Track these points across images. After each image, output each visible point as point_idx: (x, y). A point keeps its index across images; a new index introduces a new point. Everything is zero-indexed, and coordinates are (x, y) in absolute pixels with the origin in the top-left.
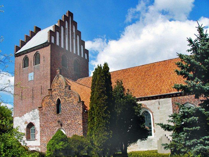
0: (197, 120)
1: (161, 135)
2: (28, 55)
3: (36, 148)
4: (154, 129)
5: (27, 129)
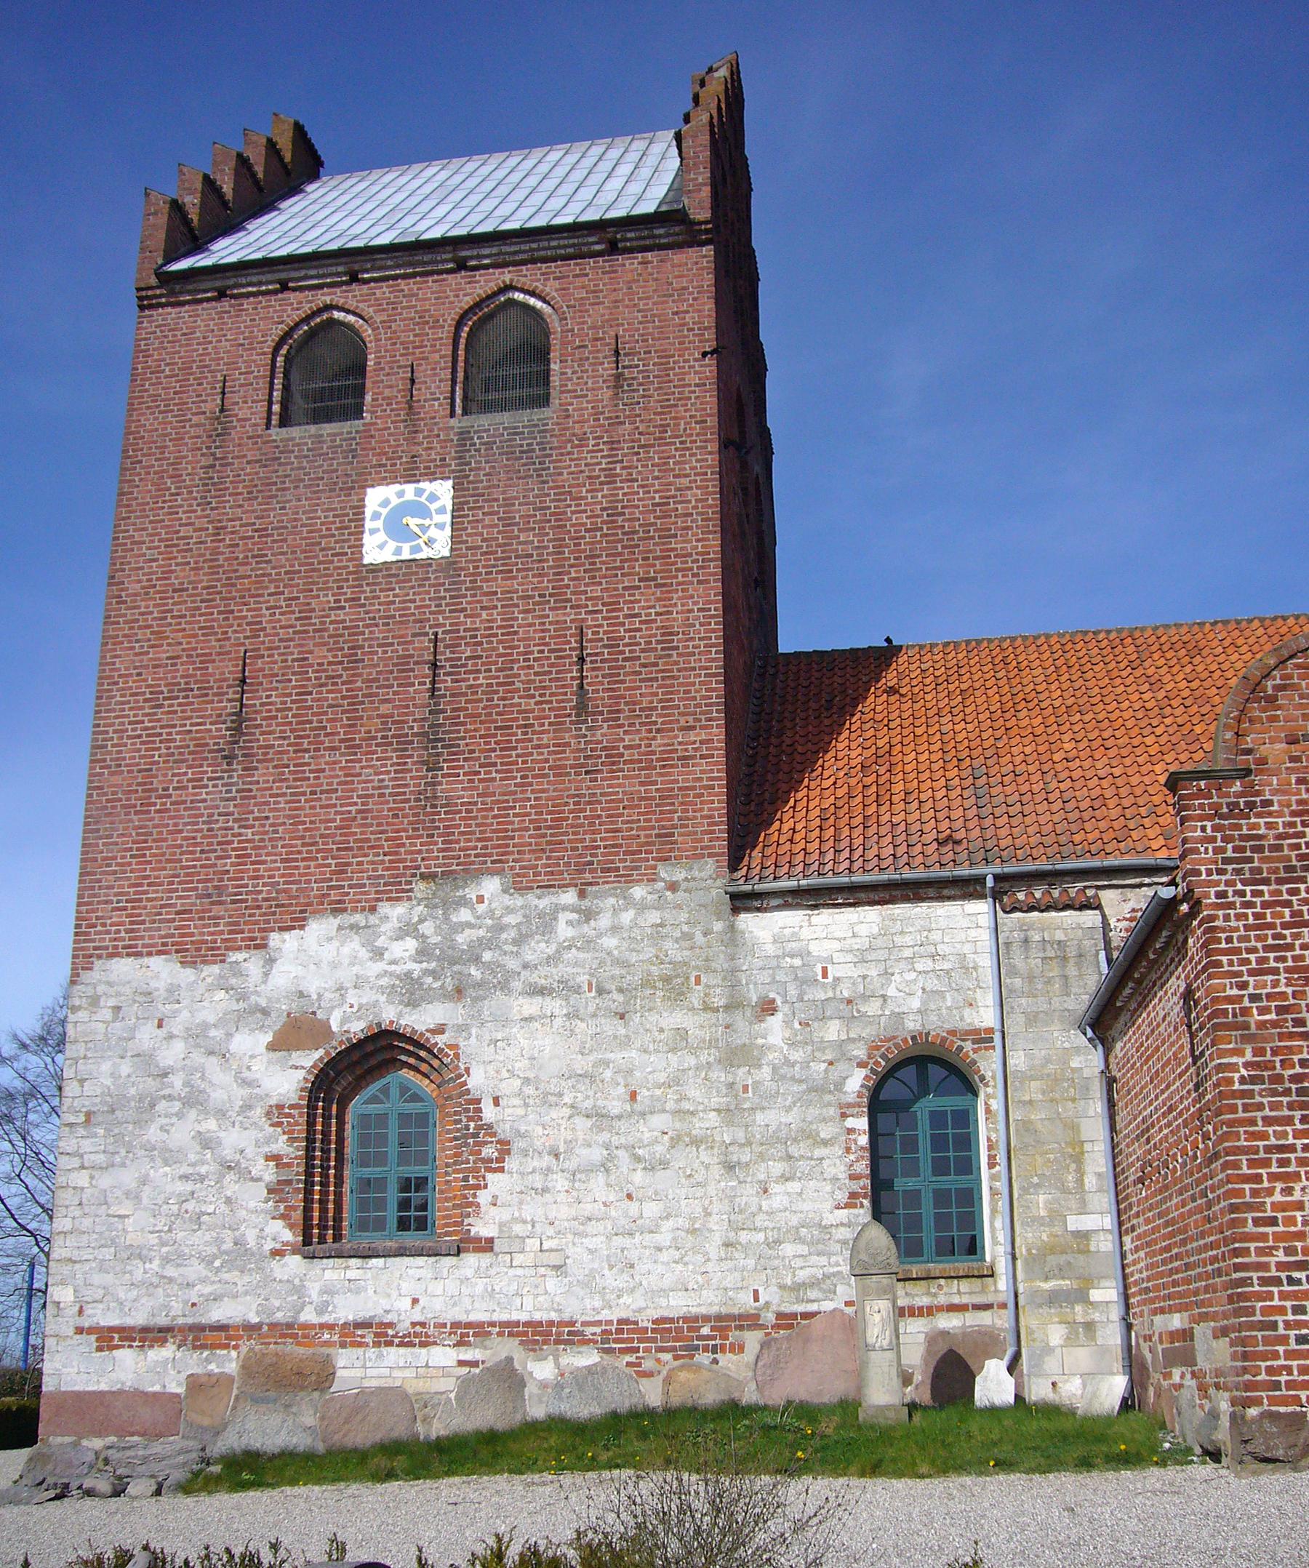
0: (726, 1360)
1: (693, 379)
2: (360, 307)
3: (468, 1354)
4: (989, 1139)
5: (311, 1107)
